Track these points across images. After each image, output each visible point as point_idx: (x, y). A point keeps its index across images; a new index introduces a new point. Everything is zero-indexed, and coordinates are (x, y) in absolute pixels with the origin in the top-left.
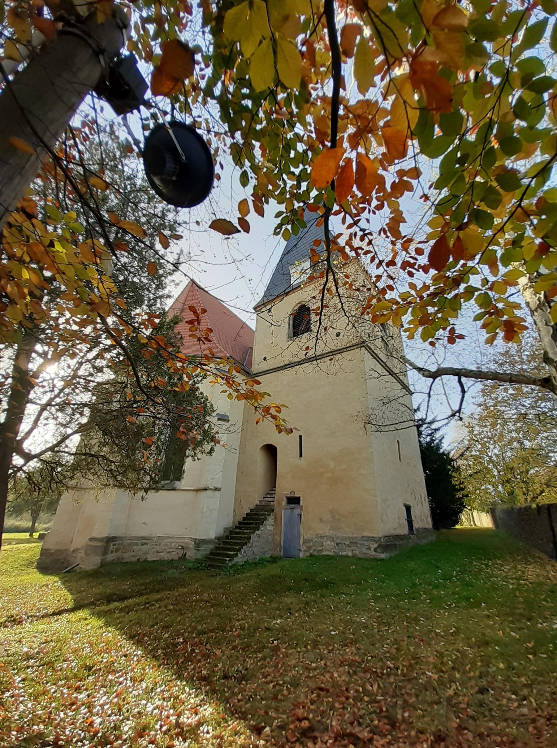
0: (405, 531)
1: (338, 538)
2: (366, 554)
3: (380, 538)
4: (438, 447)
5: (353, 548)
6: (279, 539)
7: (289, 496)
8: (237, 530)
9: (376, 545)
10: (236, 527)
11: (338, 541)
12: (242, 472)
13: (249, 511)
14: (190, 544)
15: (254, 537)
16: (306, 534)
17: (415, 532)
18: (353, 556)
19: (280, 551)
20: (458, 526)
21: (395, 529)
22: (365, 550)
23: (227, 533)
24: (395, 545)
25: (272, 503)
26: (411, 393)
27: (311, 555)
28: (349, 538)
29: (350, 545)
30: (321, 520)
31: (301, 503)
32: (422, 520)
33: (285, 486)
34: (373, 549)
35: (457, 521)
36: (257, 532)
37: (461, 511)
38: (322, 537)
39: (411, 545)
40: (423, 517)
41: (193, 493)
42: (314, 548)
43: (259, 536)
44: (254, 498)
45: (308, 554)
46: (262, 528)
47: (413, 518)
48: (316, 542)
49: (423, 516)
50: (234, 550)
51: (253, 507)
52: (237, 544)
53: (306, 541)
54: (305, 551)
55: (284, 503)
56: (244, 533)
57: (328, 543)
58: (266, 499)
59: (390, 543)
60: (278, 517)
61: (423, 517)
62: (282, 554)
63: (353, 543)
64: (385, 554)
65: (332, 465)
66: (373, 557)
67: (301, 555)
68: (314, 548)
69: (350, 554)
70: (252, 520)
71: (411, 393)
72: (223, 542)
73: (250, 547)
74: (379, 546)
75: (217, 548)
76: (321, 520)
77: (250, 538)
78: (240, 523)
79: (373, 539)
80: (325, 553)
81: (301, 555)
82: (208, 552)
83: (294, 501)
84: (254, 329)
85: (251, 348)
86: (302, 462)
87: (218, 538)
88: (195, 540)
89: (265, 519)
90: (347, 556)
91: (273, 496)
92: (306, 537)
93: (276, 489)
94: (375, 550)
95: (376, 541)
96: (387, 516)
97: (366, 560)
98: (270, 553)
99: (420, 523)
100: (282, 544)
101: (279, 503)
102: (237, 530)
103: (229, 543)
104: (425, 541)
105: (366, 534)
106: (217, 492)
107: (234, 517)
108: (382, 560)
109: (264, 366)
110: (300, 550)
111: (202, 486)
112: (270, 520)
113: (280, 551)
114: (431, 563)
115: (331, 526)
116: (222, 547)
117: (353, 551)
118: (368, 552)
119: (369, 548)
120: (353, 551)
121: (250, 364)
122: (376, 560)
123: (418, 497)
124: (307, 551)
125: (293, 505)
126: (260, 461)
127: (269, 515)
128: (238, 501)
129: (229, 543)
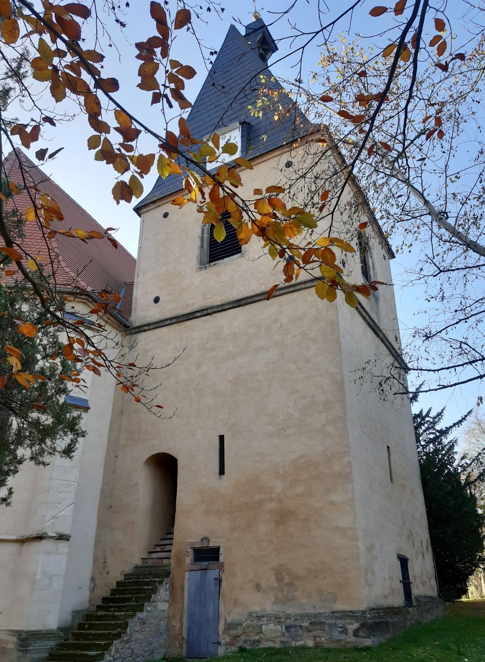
0: (399, 600)
1: (288, 617)
2: (338, 641)
3: (364, 612)
4: (443, 465)
5: (316, 633)
6: (178, 626)
7: (199, 546)
8: (100, 613)
9: (356, 625)
10: (99, 608)
11: (289, 622)
12: (110, 506)
13: (121, 578)
14: (7, 642)
15: (133, 625)
16: (229, 613)
17: (414, 603)
18: (317, 646)
19: (181, 647)
20: (464, 599)
21: (385, 597)
22: (336, 635)
23: (79, 620)
24: (387, 622)
25: (165, 562)
26: (407, 369)
27: (242, 650)
28: (307, 615)
29: (311, 628)
30: (258, 587)
31: (222, 558)
32: (424, 583)
33: (192, 526)
34: (351, 632)
35: (465, 591)
36: (139, 615)
37: (471, 573)
38: (259, 618)
39: (409, 624)
40: (425, 578)
41: (12, 548)
42: (243, 638)
43: (143, 622)
44: (132, 551)
45: (234, 649)
46: (148, 607)
47: (411, 579)
48: (248, 626)
49: (425, 579)
50: (98, 647)
51: (128, 569)
52: (101, 636)
53: (229, 627)
54: (227, 644)
55: (189, 560)
56: (114, 618)
57: (270, 629)
58: (154, 555)
59: (377, 621)
60: (177, 586)
61: (425, 578)
62: (184, 653)
63: (316, 622)
64: (373, 639)
65: (279, 486)
66: (350, 646)
67: (221, 651)
68: (243, 638)
69: (310, 643)
70: (122, 599)
71: (407, 369)
72: (74, 635)
73: (127, 642)
74: (363, 626)
75: (62, 646)
76: (258, 587)
77: (125, 626)
78: (105, 600)
79: (351, 615)
80: (265, 645)
81: (221, 651)
82: (46, 655)
83: (207, 555)
84: (134, 254)
85: (130, 286)
86: (225, 484)
87: (61, 629)
88: (18, 633)
89: (154, 591)
90: (304, 648)
91: (168, 548)
92: (229, 620)
93: (175, 536)
94: (356, 633)
95: (357, 619)
96: (373, 574)
97: (339, 651)
98: (162, 651)
99: (421, 587)
100: (185, 635)
101: (180, 561)
102: (100, 613)
103: (85, 637)
104: (429, 617)
105: (339, 607)
106: (62, 546)
107: (92, 590)
108: (367, 649)
109: (155, 314)
110: (219, 643)
111: (32, 532)
112: (163, 592)
113: (181, 647)
114: (448, 648)
115: (277, 597)
116: (75, 644)
117: (315, 637)
118: (343, 637)
119: (345, 631)
120: (315, 637)
121: (129, 311)
122: (357, 649)
123: (418, 544)
124: (232, 644)
125: (206, 563)
126: (142, 487)
127: (161, 583)
128: (100, 562)
129: (85, 637)
